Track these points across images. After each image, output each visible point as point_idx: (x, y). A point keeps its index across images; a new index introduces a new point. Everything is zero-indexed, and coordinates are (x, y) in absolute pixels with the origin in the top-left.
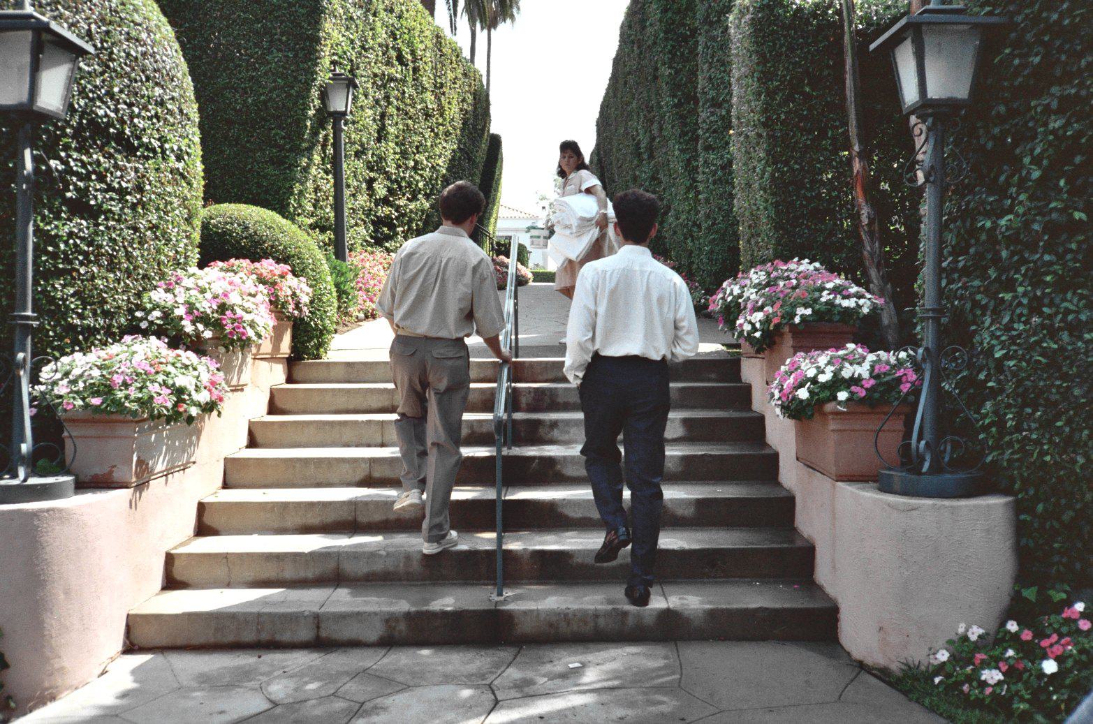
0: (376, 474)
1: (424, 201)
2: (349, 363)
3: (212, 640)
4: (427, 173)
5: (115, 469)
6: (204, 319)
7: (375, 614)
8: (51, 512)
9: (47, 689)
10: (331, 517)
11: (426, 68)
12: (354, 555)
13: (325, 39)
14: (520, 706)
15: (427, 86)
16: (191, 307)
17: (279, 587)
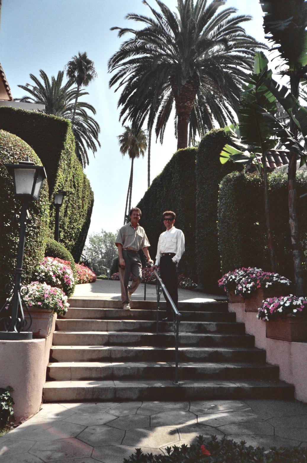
0: (111, 341)
1: (73, 242)
2: (84, 300)
3: (75, 398)
4: (76, 230)
5: (40, 331)
6: (58, 277)
7: (136, 388)
8: (32, 344)
9: (26, 413)
10: (101, 355)
11: (81, 189)
12: (119, 368)
13: (58, 176)
14: (206, 416)
15: (80, 197)
16: (54, 273)
17: (94, 380)
